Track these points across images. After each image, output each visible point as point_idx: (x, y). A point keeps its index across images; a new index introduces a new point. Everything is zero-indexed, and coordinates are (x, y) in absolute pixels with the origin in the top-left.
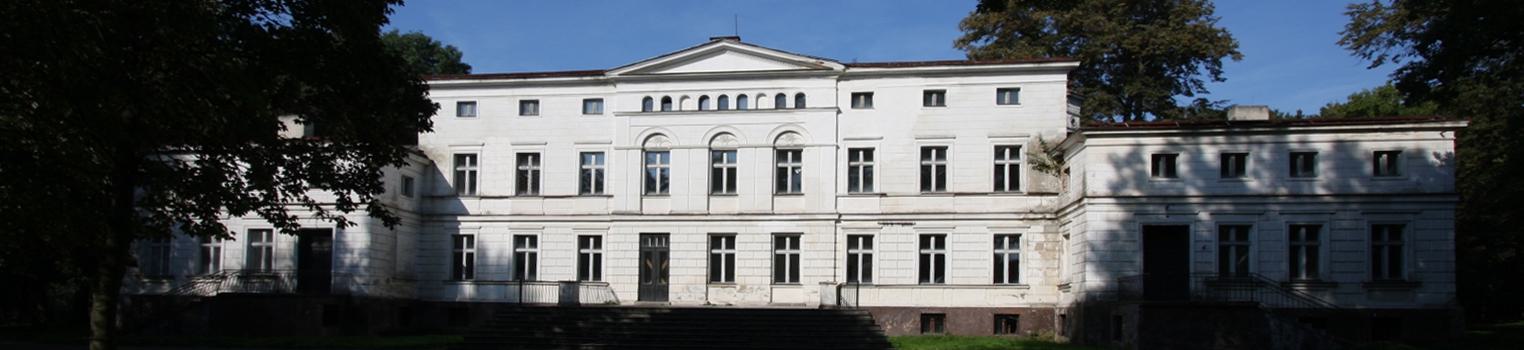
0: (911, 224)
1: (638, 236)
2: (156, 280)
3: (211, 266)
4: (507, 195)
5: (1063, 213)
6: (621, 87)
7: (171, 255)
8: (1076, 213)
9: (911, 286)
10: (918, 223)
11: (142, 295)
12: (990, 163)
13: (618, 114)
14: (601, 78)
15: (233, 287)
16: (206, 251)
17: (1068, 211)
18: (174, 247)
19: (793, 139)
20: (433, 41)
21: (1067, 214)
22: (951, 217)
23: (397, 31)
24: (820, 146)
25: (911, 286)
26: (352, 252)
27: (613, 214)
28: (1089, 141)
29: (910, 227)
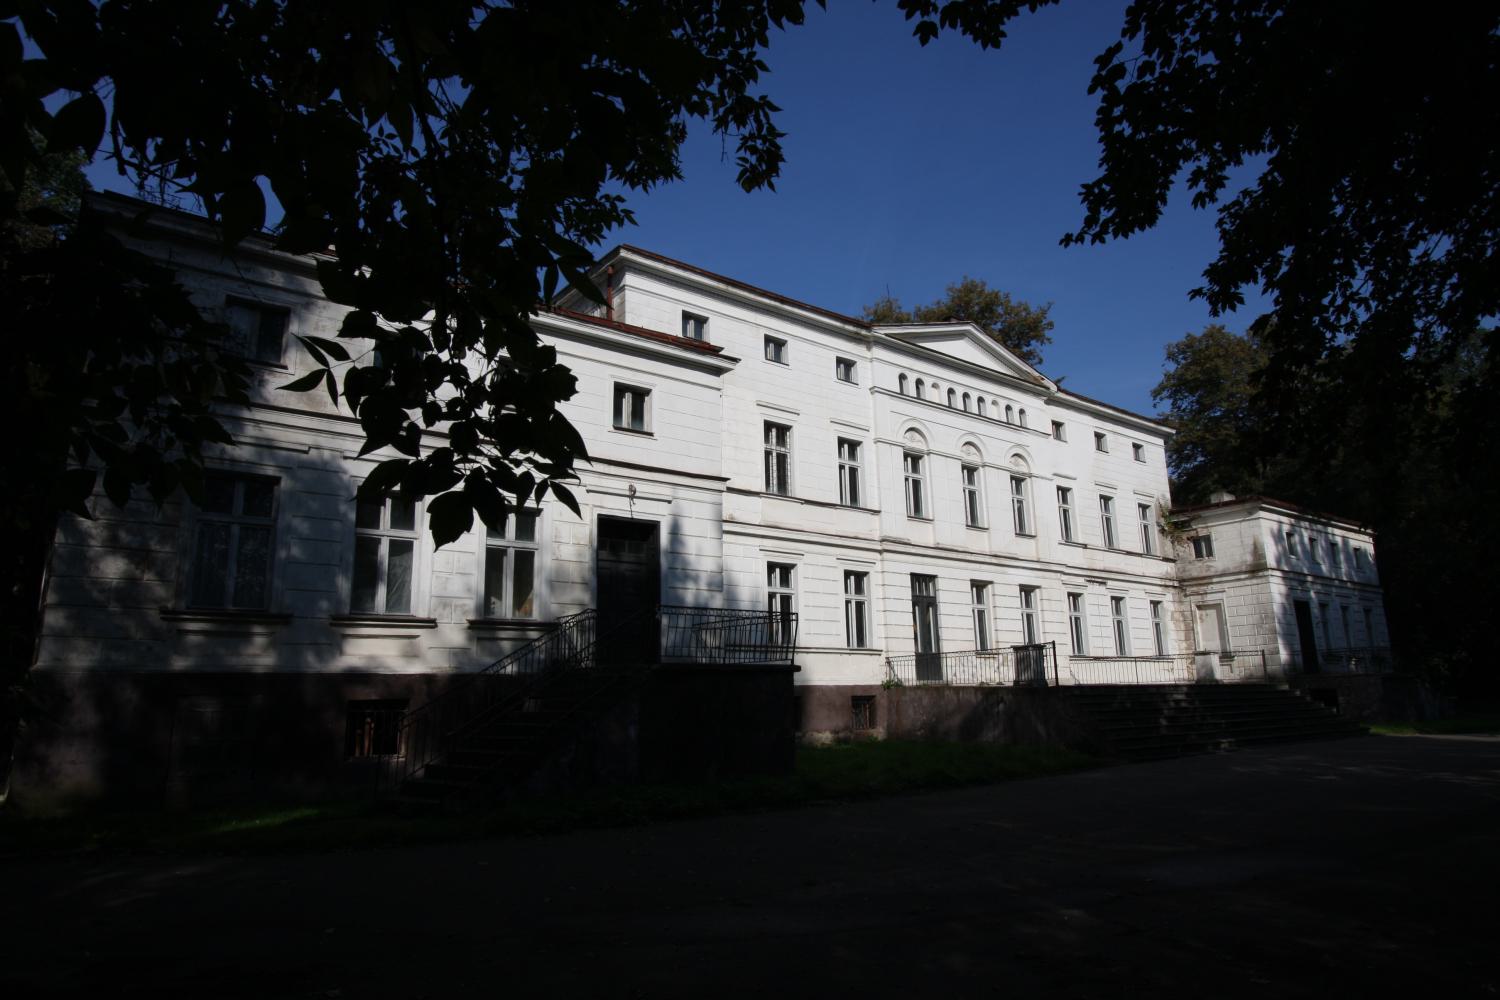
0: (1104, 583)
1: (908, 581)
2: (234, 627)
3: (382, 592)
4: (753, 489)
5: (1209, 581)
6: (878, 352)
7: (282, 554)
8: (1232, 584)
9: (838, 651)
10: (1109, 583)
11: (184, 675)
13: (873, 390)
14: (864, 332)
15: (458, 653)
16: (369, 546)
17: (1215, 580)
18: (289, 529)
19: (260, 429)
20: (1147, 228)
21: (1212, 583)
23: (783, 160)
24: (1042, 478)
25: (838, 651)
26: (696, 580)
27: (883, 541)
28: (1262, 514)
29: (1103, 588)
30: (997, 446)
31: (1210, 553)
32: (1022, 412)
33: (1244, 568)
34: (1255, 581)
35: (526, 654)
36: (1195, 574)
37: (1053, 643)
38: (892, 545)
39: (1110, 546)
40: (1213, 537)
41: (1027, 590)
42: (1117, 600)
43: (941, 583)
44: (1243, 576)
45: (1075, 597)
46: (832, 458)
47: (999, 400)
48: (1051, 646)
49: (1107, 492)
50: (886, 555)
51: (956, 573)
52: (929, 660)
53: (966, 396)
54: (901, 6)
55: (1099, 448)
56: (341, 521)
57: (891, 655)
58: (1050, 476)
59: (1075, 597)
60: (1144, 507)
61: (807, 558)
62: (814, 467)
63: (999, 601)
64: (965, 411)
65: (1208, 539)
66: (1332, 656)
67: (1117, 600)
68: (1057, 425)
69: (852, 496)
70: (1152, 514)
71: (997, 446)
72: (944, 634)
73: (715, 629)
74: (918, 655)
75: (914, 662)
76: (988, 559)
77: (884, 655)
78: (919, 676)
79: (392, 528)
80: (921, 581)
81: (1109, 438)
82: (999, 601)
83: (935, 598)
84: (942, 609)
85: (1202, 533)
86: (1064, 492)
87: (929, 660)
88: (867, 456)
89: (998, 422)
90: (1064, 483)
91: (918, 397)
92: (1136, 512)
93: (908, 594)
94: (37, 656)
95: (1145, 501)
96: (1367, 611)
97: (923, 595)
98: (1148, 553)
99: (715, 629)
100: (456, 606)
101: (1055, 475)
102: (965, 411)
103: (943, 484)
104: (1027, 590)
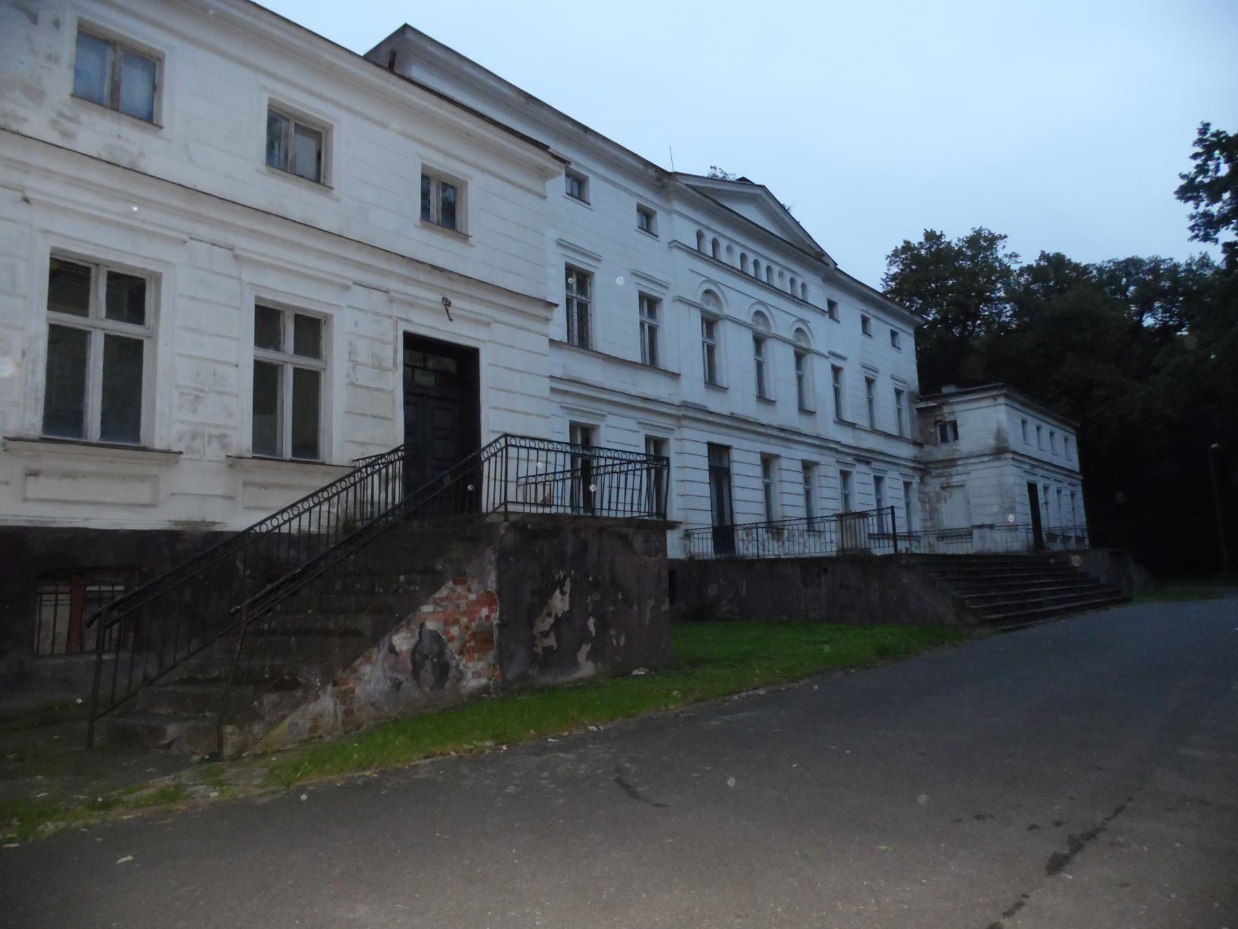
1: (704, 450)
10: (874, 464)
12: (243, 352)
22: (753, 428)
30: (783, 320)
31: (956, 437)
32: (804, 286)
33: (987, 452)
34: (997, 464)
35: (290, 520)
36: (940, 457)
37: (892, 508)
38: (694, 413)
39: (874, 431)
40: (958, 423)
41: (807, 466)
42: (878, 480)
43: (735, 455)
44: (986, 459)
45: (845, 475)
46: (633, 315)
47: (786, 272)
48: (889, 511)
49: (871, 375)
50: (685, 423)
51: (747, 444)
52: (724, 533)
53: (756, 263)
54: (1213, 143)
55: (865, 331)
56: (24, 297)
57: (689, 527)
58: (826, 353)
59: (845, 475)
60: (898, 393)
61: (611, 420)
62: (615, 325)
63: (786, 475)
64: (699, 251)
65: (954, 425)
66: (1052, 537)
67: (878, 480)
68: (832, 304)
69: (651, 361)
70: (904, 398)
71: (783, 320)
72: (737, 507)
73: (536, 484)
74: (714, 528)
75: (710, 535)
76: (776, 433)
77: (683, 527)
78: (716, 552)
79: (107, 317)
80: (718, 453)
81: (873, 322)
82: (786, 475)
83: (728, 469)
84: (736, 481)
85: (949, 418)
86: (836, 371)
87: (724, 533)
88: (725, 332)
89: (730, 269)
90: (838, 363)
91: (714, 258)
92: (893, 395)
93: (704, 464)
94: (1029, 407)
95: (901, 387)
96: (1073, 495)
97: (720, 475)
98: (900, 438)
99: (621, 472)
100: (210, 436)
101: (830, 353)
102: (714, 258)
103: (735, 347)
104: (807, 466)
